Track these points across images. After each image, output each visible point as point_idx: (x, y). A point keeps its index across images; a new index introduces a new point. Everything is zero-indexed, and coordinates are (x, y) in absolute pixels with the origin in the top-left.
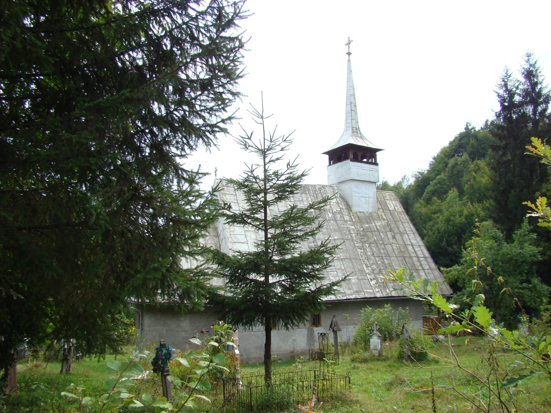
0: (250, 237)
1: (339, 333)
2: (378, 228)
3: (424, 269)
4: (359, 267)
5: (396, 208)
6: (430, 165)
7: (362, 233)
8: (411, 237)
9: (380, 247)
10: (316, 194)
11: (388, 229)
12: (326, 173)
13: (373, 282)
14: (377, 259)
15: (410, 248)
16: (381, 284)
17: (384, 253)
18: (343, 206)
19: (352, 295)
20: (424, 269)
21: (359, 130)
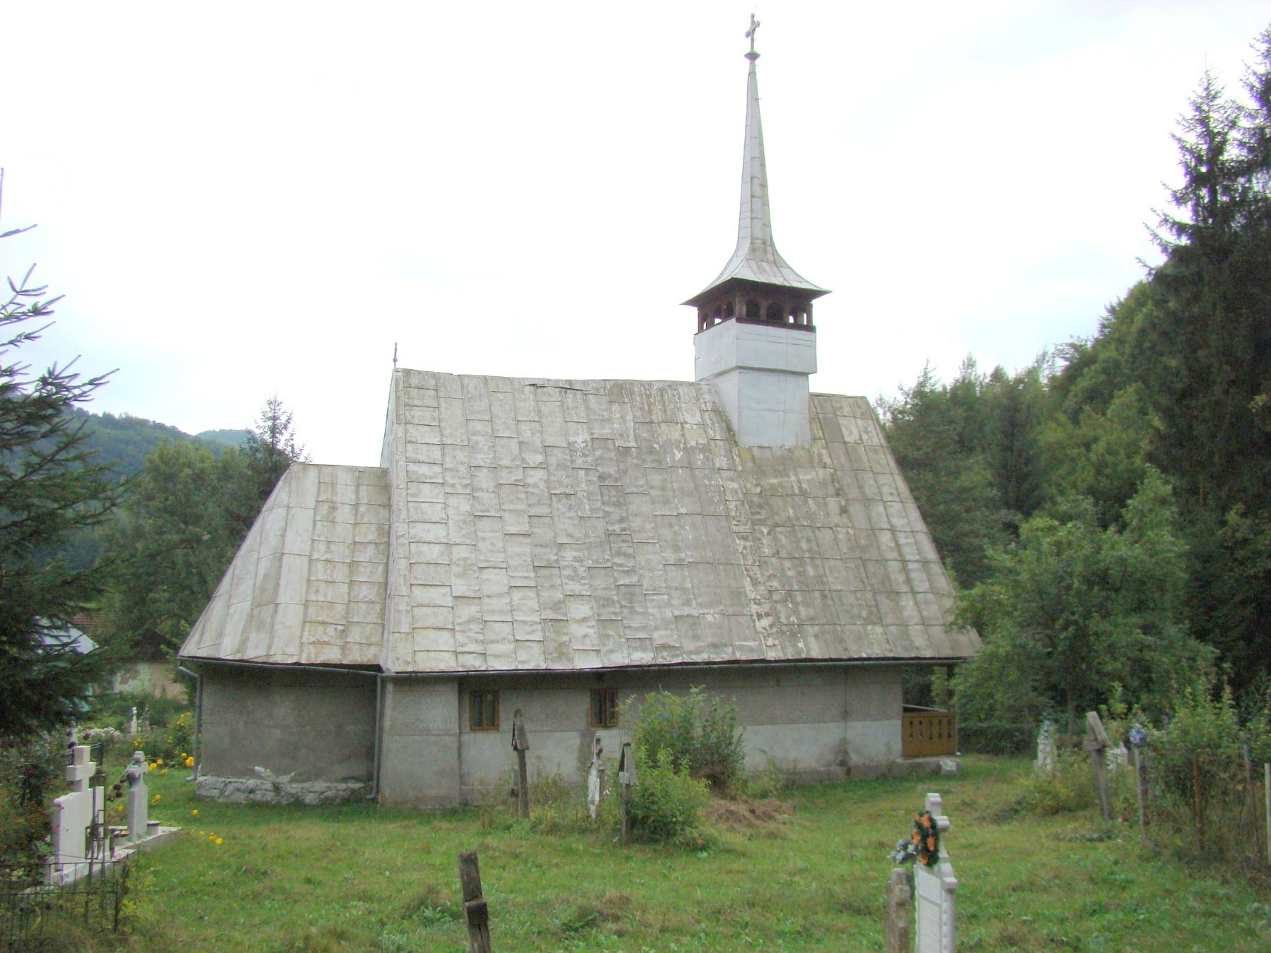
0: (457, 508)
1: (527, 753)
2: (804, 486)
3: (914, 592)
4: (733, 584)
5: (865, 437)
6: (1104, 326)
7: (756, 499)
8: (891, 511)
9: (799, 535)
10: (649, 405)
11: (831, 490)
12: (691, 351)
13: (765, 622)
14: (787, 564)
15: (885, 538)
16: (784, 628)
17: (810, 551)
18: (717, 433)
19: (698, 652)
20: (914, 592)
21: (772, 244)
